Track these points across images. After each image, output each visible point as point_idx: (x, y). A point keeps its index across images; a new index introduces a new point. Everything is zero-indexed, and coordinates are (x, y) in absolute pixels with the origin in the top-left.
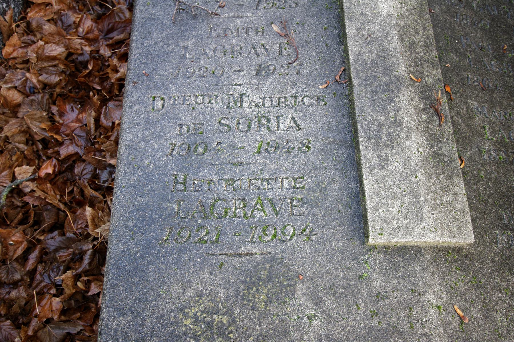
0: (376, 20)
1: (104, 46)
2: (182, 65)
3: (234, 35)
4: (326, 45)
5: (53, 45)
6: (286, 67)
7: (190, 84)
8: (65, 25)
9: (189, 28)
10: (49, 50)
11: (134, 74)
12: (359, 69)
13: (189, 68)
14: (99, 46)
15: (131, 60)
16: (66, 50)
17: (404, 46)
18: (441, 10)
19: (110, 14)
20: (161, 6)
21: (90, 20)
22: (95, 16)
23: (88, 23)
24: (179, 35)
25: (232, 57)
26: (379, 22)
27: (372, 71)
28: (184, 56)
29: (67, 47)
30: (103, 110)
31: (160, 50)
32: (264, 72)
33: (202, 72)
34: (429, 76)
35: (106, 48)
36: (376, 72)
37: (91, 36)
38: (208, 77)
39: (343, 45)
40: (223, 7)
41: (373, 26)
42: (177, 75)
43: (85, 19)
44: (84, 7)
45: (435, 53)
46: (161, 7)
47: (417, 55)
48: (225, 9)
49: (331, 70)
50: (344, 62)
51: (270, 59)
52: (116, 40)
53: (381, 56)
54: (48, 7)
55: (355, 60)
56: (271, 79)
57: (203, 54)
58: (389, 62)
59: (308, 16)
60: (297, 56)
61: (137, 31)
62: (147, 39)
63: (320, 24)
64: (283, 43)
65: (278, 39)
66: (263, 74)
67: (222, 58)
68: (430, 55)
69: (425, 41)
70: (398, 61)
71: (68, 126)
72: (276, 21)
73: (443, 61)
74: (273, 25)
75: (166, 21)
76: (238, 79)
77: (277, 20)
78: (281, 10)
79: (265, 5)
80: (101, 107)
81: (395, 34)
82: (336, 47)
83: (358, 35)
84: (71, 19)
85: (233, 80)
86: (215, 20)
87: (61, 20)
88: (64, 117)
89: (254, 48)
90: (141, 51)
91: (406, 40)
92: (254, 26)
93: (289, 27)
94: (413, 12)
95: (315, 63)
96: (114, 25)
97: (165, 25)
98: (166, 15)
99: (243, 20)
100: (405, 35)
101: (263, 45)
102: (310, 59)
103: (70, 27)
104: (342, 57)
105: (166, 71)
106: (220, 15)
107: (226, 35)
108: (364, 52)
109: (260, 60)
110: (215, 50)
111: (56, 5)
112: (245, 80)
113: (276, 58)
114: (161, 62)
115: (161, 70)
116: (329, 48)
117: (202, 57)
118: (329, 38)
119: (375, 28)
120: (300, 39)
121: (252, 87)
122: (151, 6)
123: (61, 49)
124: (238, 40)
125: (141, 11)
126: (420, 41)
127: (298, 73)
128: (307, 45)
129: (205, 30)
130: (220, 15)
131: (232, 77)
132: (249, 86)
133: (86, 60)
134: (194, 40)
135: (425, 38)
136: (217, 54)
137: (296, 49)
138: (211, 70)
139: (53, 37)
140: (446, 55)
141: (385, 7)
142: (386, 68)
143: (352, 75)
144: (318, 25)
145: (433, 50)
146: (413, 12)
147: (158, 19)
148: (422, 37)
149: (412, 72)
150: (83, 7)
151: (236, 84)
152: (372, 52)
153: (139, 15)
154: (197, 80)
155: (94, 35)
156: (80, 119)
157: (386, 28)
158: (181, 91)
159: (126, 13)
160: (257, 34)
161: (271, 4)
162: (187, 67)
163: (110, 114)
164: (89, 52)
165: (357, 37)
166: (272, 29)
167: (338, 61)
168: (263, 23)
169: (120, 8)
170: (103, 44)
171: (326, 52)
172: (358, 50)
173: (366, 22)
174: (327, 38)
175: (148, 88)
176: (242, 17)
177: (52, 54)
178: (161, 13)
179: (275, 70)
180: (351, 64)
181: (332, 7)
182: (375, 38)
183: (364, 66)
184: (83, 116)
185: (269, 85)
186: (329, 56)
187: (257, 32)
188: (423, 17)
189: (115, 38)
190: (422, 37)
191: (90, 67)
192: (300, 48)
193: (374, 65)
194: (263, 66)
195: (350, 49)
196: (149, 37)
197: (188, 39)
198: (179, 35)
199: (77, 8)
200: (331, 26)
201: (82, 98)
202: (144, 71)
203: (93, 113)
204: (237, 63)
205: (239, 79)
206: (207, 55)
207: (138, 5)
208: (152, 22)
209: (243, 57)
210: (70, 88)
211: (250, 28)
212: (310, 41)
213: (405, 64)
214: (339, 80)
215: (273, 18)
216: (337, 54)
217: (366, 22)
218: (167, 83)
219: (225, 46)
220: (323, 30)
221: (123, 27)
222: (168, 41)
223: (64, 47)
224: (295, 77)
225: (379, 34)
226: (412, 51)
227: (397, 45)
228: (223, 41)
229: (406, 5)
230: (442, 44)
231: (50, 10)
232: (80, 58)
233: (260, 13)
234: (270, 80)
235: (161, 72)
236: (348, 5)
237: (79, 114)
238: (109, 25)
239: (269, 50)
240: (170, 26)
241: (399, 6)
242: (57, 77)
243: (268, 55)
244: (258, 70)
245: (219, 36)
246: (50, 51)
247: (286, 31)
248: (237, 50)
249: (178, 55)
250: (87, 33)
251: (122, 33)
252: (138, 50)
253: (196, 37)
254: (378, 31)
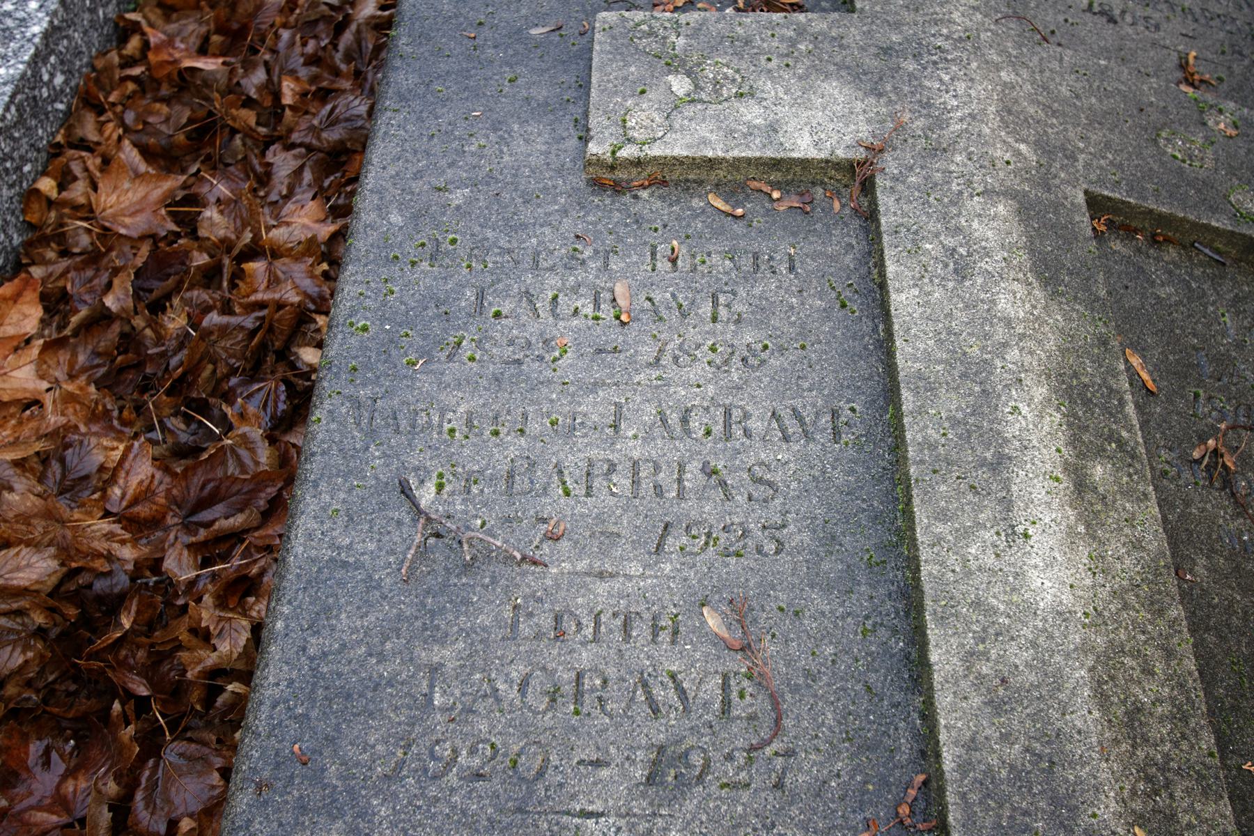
0: (1020, 626)
1: (179, 546)
2: (418, 729)
3: (585, 637)
4: (869, 689)
5: (25, 551)
6: (742, 761)
7: (437, 800)
8: (72, 477)
9: (451, 602)
10: (9, 567)
11: (264, 750)
12: (974, 797)
13: (437, 742)
14: (163, 541)
15: (261, 703)
16: (62, 565)
17: (1110, 721)
18: (1212, 569)
19: (211, 456)
20: (370, 521)
21: (149, 463)
22: (167, 450)
23: (142, 471)
24: (418, 624)
25: (577, 713)
26: (1031, 637)
27: (1014, 809)
28: (429, 697)
29: (65, 553)
30: (147, 773)
31: (354, 672)
32: (672, 772)
33: (477, 761)
34: (1194, 827)
35: (186, 553)
36: (1026, 813)
37: (143, 510)
38: (496, 781)
39: (921, 695)
40: (558, 539)
41: (1013, 648)
42: (401, 764)
43: (135, 457)
44: (138, 416)
45: (1207, 741)
46: (371, 528)
47: (1152, 752)
48: (564, 544)
49: (884, 782)
50: (923, 753)
51: (692, 728)
52: (217, 531)
53: (1040, 757)
54: (28, 412)
55: (959, 766)
56: (695, 802)
57: (486, 696)
58: (1066, 781)
59: (812, 587)
60: (778, 721)
61: (290, 602)
62: (318, 632)
63: (849, 614)
64: (736, 674)
65: (719, 658)
66: (670, 779)
67: (544, 712)
68: (1192, 747)
69: (1172, 699)
70: (1095, 778)
71: (21, 821)
72: (717, 597)
73: (1232, 752)
74: (705, 610)
75: (383, 574)
76: (591, 792)
77: (719, 592)
78: (733, 560)
79: (684, 540)
80: (142, 760)
81: (1081, 682)
82: (898, 697)
83: (966, 676)
84: (94, 458)
85: (573, 797)
86: (531, 580)
87: (62, 461)
88: (15, 787)
89: (645, 685)
90: (294, 674)
91: (1116, 700)
92: (648, 609)
93: (755, 620)
94: (1131, 598)
95: (833, 755)
96: (217, 488)
97: (378, 587)
98: (383, 553)
99: (617, 584)
100: (1111, 683)
101: (673, 676)
102: (817, 736)
103: (85, 483)
104: (916, 736)
105: (365, 751)
106: (546, 566)
107: (560, 635)
108: (986, 738)
109: (663, 729)
110: (524, 685)
111: (55, 412)
112: (611, 796)
113: (711, 727)
114: (355, 715)
115: (351, 744)
116: (876, 699)
117: (480, 706)
118: (876, 665)
119: (1019, 655)
120: (788, 665)
121: (634, 825)
122: (342, 520)
123: (45, 565)
124: (596, 655)
125: (310, 537)
126: (1157, 700)
127: (779, 786)
128: (809, 686)
129: (498, 614)
130: (546, 566)
131: (573, 785)
132: (622, 823)
133: (116, 590)
134: (461, 645)
135: (1173, 689)
136: (530, 699)
137: (775, 700)
138: (505, 755)
139: (29, 524)
140: (1241, 728)
141: (1048, 584)
142: (1055, 801)
143: (951, 819)
144: (843, 618)
145: (1202, 727)
146: (1131, 598)
147: (358, 566)
148: (1163, 686)
149: (1142, 816)
150: (134, 415)
151: (582, 811)
152: (1012, 738)
153: (300, 549)
154: (461, 787)
155: (154, 507)
156: (65, 797)
157: (1051, 656)
158: (407, 826)
159: (259, 451)
160: (655, 635)
161: (703, 538)
162: (434, 738)
163: (166, 790)
164: (130, 567)
165: (963, 683)
166: (704, 623)
167: (906, 747)
168: (676, 599)
169: (244, 436)
170: (176, 538)
171: (867, 716)
172: (969, 727)
173: (991, 631)
174: (870, 668)
175: (303, 808)
176: (612, 576)
177: (15, 582)
178: (371, 546)
179: (706, 766)
180: (947, 776)
181: (884, 562)
182: (1018, 690)
183: (988, 785)
184: (77, 786)
185: (689, 824)
186: (876, 731)
187: (656, 630)
188: (1161, 612)
189: (216, 526)
190: (1163, 686)
191: (126, 623)
192: (788, 697)
193: (1020, 787)
194: (669, 751)
195: (943, 722)
196: (324, 627)
197: (442, 642)
198: (418, 624)
199: (116, 413)
200: (882, 625)
201: (83, 718)
202: (297, 746)
203: (112, 788)
204: (589, 734)
205: (595, 794)
206: (498, 700)
207: (302, 513)
208: (339, 574)
209: (611, 717)
210: (51, 678)
211: (637, 613)
212: (819, 672)
213: (1117, 787)
214: (908, 822)
215: (706, 587)
216: (902, 724)
217: (991, 631)
218: (363, 792)
219: (556, 670)
220: (860, 637)
221: (245, 493)
222: (383, 643)
223: (55, 557)
224: (770, 799)
225: (1032, 678)
226: (1135, 737)
227: (1089, 717)
228: (551, 654)
229: (1109, 578)
230: (1226, 689)
231: (33, 424)
232: (100, 585)
233: (668, 568)
234: (690, 805)
235: (351, 752)
236: (935, 569)
237: (64, 778)
238: (203, 487)
239: (691, 695)
240: (391, 591)
241: (1088, 582)
242: (16, 654)
243: (686, 710)
244: (654, 763)
245: (538, 636)
246: (11, 571)
247: (744, 633)
248: (593, 689)
249: (408, 694)
250: (135, 501)
251: (241, 510)
252: (286, 668)
253: (468, 635)
254: (1027, 665)
